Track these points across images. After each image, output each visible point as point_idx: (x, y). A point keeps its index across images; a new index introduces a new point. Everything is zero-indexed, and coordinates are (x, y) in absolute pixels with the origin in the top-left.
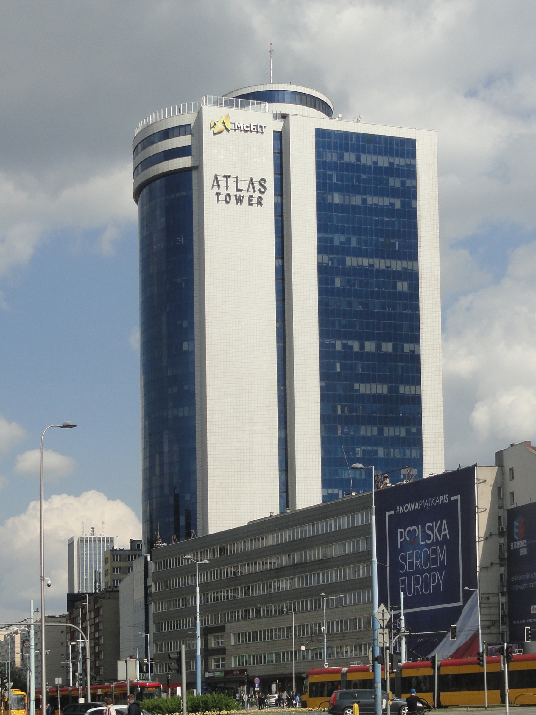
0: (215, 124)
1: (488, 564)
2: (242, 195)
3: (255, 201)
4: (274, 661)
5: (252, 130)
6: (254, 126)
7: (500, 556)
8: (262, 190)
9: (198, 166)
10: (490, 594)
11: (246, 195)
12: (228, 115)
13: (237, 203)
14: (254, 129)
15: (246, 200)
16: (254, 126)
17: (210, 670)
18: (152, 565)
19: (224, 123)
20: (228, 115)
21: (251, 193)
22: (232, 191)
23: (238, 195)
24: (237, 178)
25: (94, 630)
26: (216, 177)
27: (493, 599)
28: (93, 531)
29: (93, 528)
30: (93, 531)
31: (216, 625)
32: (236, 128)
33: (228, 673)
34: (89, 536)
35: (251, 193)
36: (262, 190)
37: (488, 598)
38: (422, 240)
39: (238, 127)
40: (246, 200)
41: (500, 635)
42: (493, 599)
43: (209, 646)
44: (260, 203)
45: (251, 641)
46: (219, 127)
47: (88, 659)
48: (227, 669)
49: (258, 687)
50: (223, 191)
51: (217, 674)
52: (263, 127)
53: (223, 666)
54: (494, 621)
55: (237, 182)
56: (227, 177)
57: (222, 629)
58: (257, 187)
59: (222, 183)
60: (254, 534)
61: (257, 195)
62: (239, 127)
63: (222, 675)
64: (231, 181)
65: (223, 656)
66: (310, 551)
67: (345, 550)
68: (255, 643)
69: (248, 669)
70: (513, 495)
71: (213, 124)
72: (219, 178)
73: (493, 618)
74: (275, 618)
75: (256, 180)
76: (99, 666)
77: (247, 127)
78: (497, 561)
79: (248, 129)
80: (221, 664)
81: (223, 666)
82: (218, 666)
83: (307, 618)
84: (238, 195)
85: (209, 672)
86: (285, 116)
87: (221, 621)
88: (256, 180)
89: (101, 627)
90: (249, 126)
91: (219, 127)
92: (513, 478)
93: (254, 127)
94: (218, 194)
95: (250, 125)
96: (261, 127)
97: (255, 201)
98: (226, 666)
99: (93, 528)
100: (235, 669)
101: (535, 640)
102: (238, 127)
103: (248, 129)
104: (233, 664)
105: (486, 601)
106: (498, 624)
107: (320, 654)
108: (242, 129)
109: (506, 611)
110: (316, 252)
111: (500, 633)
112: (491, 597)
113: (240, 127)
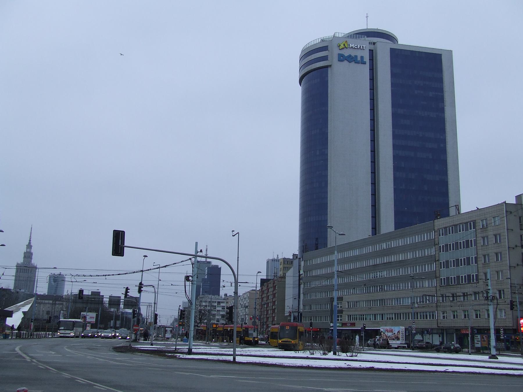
0: (340, 45)
6: (359, 46)
9: (331, 65)
12: (346, 41)
16: (359, 46)
18: (52, 355)
20: (346, 41)
25: (273, 297)
28: (278, 256)
29: (278, 255)
30: (278, 256)
32: (350, 47)
34: (276, 258)
45: (419, 319)
46: (342, 46)
53: (341, 320)
60: (424, 231)
62: (352, 46)
65: (341, 314)
66: (428, 249)
67: (399, 258)
68: (422, 320)
71: (339, 45)
74: (372, 294)
76: (275, 309)
79: (356, 48)
80: (340, 319)
81: (341, 320)
86: (374, 44)
87: (340, 295)
89: (276, 303)
90: (357, 46)
93: (360, 47)
95: (358, 46)
99: (278, 255)
101: (2, 289)
103: (356, 48)
107: (433, 315)
108: (353, 47)
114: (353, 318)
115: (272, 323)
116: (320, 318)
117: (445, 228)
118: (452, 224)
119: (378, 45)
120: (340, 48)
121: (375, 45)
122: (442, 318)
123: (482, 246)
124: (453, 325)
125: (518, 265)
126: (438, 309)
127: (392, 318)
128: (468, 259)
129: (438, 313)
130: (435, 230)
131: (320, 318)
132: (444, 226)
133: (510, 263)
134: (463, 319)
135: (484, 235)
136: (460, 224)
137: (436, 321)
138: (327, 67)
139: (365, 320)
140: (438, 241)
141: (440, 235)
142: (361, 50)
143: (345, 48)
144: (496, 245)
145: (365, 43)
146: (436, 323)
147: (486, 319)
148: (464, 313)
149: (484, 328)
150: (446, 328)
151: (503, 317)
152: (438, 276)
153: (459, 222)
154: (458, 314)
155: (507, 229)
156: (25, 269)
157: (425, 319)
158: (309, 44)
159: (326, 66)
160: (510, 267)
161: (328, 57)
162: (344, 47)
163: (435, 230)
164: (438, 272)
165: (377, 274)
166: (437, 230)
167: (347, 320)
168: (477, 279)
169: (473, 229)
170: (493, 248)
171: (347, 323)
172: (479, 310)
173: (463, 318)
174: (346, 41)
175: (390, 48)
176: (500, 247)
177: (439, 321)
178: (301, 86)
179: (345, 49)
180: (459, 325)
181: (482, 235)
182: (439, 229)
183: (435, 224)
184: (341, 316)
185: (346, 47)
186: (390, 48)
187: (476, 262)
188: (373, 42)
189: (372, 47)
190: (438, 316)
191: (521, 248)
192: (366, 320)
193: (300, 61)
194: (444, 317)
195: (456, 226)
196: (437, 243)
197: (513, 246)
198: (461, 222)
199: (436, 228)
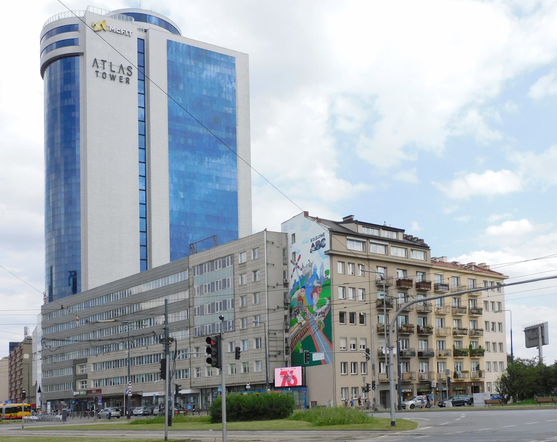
0: (95, 25)
1: (275, 307)
2: (114, 75)
3: (124, 80)
4: (120, 383)
5: (122, 33)
7: (284, 302)
8: (129, 73)
10: (276, 330)
11: (118, 76)
13: (111, 79)
14: (123, 33)
15: (117, 79)
17: (77, 390)
19: (101, 25)
21: (121, 75)
22: (108, 72)
23: (112, 74)
24: (111, 63)
26: (95, 60)
27: (279, 335)
31: (82, 358)
32: (111, 30)
33: (89, 392)
35: (121, 75)
36: (129, 73)
37: (275, 334)
38: (239, 121)
39: (112, 30)
40: (117, 79)
41: (285, 362)
42: (279, 335)
43: (77, 373)
44: (128, 81)
47: (551, 405)
48: (88, 390)
49: (100, 402)
50: (101, 71)
51: (82, 393)
52: (130, 33)
54: (280, 351)
55: (111, 66)
56: (104, 61)
57: (85, 360)
58: (126, 71)
59: (100, 65)
61: (125, 77)
62: (113, 30)
63: (85, 393)
64: (107, 65)
69: (102, 389)
70: (295, 236)
71: (93, 25)
72: (98, 61)
73: (279, 349)
75: (125, 66)
77: (118, 30)
78: (282, 305)
82: (83, 387)
83: (186, 364)
84: (112, 74)
85: (76, 391)
86: (146, 31)
87: (85, 355)
88: (125, 66)
91: (98, 27)
92: (295, 242)
93: (124, 32)
94: (97, 72)
96: (129, 32)
97: (124, 80)
98: (87, 387)
100: (93, 389)
102: (112, 30)
104: (92, 385)
105: (273, 336)
106: (283, 353)
108: (115, 31)
109: (289, 344)
110: (167, 120)
111: (284, 361)
112: (277, 332)
113: (114, 30)
114: (137, 379)
115: (20, 396)
116: (69, 385)
117: (201, 265)
118: (209, 260)
119: (150, 32)
120: (96, 29)
121: (147, 32)
122: (195, 376)
123: (240, 286)
124: (207, 384)
125: (278, 307)
126: (191, 366)
127: (119, 383)
128: (225, 302)
129: (191, 370)
130: (190, 268)
131: (69, 385)
132: (200, 263)
133: (268, 305)
134: (219, 376)
135: (243, 271)
136: (217, 259)
137: (190, 380)
138: (77, 55)
139: (182, 378)
140: (193, 283)
141: (194, 275)
142: (113, 33)
143: (103, 30)
144: (254, 284)
145: (133, 27)
146: (190, 383)
147: (241, 374)
148: (244, 366)
149: (239, 385)
150: (202, 388)
151: (260, 371)
152: (192, 325)
153: (216, 257)
154: (249, 366)
155: (267, 264)
156: (269, 340)
157: (185, 378)
158: (52, 18)
159: (76, 53)
160: (268, 309)
161: (79, 41)
162: (101, 28)
163: (190, 268)
164: (192, 320)
165: (126, 328)
166: (192, 268)
167: (92, 386)
168: (234, 327)
169: (231, 265)
170: (251, 288)
171: (92, 390)
172: (235, 364)
173: (219, 374)
174: (104, 21)
175: (167, 40)
176: (258, 286)
177: (193, 380)
178: (43, 78)
179: (102, 32)
180: (213, 384)
181: (241, 272)
182: (194, 267)
183: (190, 260)
184: (86, 382)
185: (104, 29)
186: (167, 40)
187: (233, 306)
188: (145, 29)
189: (142, 35)
190: (192, 374)
191: (283, 286)
192: (137, 382)
193: (41, 41)
194: (198, 375)
195: (212, 261)
196: (192, 285)
197: (275, 285)
198: (218, 257)
199: (191, 266)
